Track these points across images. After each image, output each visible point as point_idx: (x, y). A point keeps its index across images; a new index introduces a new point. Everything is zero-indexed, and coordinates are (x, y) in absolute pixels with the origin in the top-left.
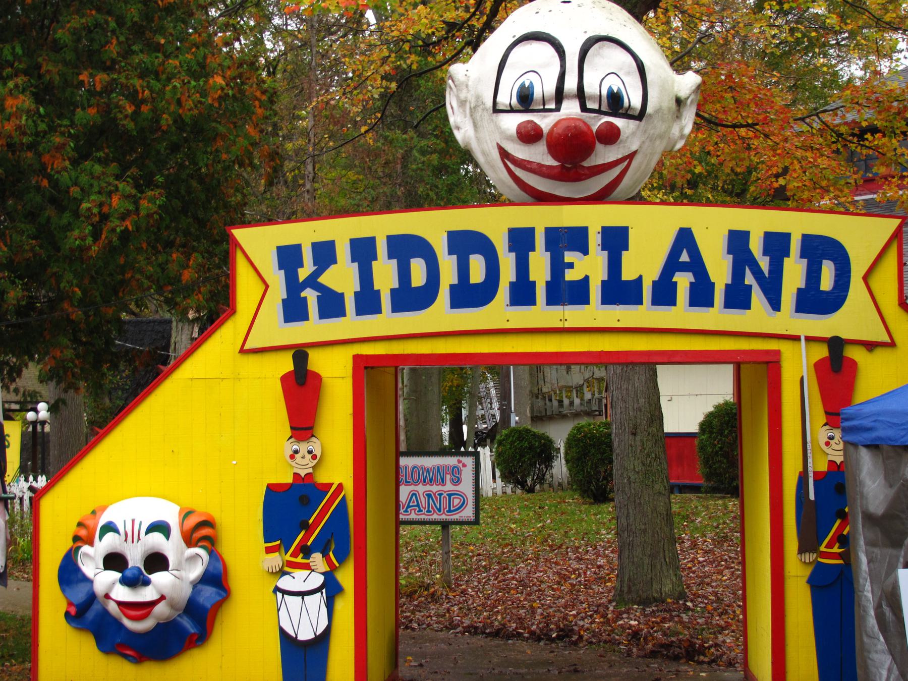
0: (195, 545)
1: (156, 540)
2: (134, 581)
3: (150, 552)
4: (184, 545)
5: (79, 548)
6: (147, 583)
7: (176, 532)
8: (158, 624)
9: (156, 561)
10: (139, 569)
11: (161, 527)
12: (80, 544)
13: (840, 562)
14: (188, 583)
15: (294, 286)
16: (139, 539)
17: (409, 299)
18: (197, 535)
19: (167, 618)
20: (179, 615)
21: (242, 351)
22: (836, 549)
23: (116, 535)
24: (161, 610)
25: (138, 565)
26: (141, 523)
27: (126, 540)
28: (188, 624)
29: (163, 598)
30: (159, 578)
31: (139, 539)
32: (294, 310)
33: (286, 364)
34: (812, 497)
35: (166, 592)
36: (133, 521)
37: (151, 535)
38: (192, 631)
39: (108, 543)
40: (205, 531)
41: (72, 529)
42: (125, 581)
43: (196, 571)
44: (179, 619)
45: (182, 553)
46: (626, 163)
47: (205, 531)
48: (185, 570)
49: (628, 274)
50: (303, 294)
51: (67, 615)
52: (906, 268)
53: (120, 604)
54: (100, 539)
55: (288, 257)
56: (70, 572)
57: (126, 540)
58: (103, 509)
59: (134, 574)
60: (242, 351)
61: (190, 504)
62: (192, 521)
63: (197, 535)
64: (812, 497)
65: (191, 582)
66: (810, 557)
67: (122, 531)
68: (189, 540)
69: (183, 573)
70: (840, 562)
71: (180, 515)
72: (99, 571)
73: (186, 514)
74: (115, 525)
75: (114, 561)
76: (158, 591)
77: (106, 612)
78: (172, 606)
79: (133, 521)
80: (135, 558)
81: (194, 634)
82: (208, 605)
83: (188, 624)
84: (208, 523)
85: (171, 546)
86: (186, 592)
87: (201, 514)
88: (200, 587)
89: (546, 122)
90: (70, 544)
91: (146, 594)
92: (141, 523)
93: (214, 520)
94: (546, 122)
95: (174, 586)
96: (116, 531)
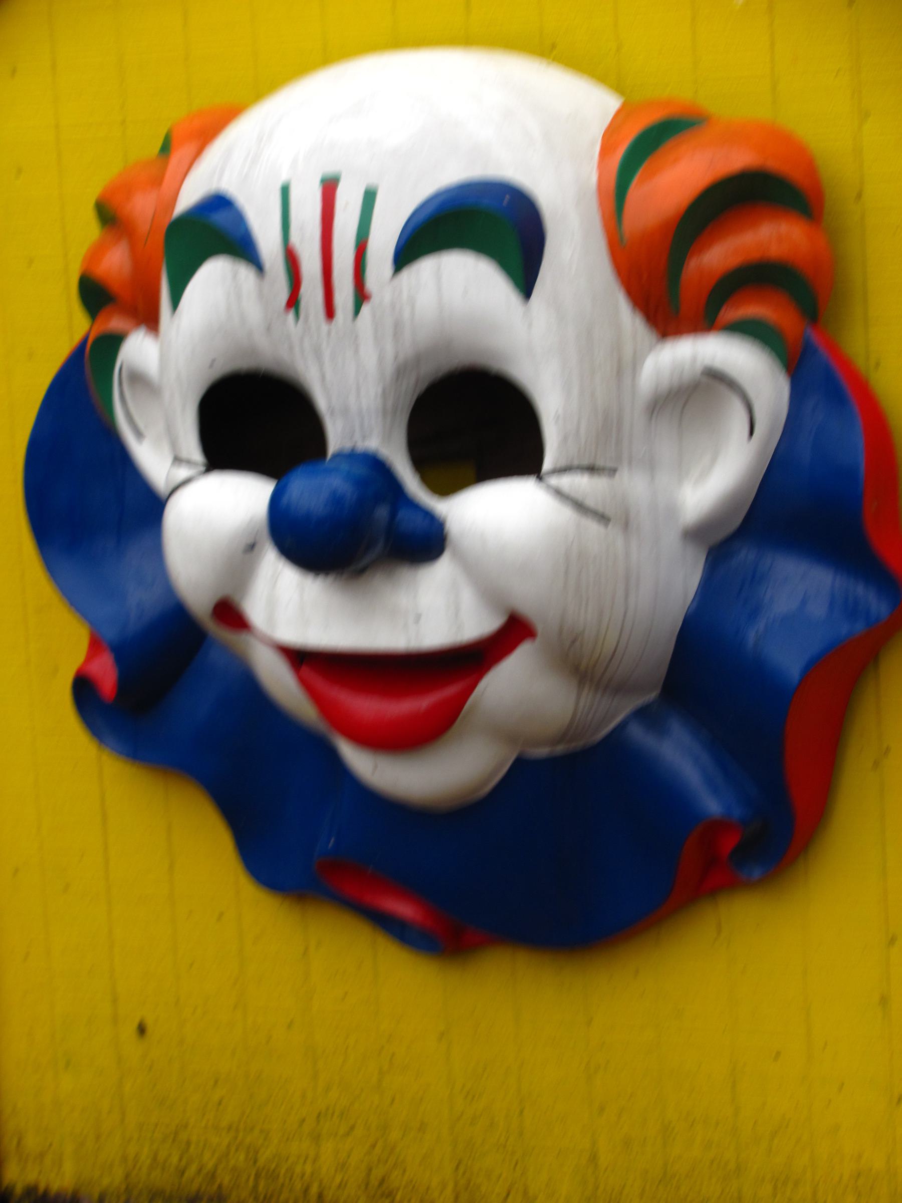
0: (705, 320)
1: (463, 286)
2: (356, 532)
3: (430, 370)
4: (629, 321)
5: (111, 343)
6: (425, 543)
7: (575, 246)
8: (522, 767)
9: (476, 420)
10: (377, 467)
11: (490, 222)
12: (116, 323)
14: (671, 540)
16: (361, 295)
18: (718, 255)
19: (563, 736)
20: (642, 714)
23: (245, 273)
24: (513, 686)
25: (373, 443)
26: (370, 197)
27: (293, 302)
28: (680, 756)
29: (514, 631)
30: (495, 514)
31: (361, 295)
35: (529, 599)
36: (329, 188)
37: (408, 274)
38: (712, 806)
39: (208, 319)
40: (770, 236)
41: (72, 239)
42: (304, 540)
43: (716, 474)
44: (638, 733)
45: (624, 369)
47: (770, 236)
48: (651, 465)
51: (83, 690)
52: (600, 463)
53: (299, 658)
54: (175, 301)
57: (293, 302)
58: (207, 128)
59: (336, 500)
61: (673, 82)
62: (680, 177)
63: (718, 255)
65: (695, 534)
67: (268, 241)
68: (664, 284)
69: (634, 485)
71: (606, 150)
72: (183, 473)
73: (645, 141)
74: (239, 219)
75: (251, 417)
76: (489, 593)
77: (249, 688)
78: (579, 665)
79: (329, 188)
80: (357, 404)
81: (717, 827)
82: (789, 660)
83: (680, 756)
84: (770, 187)
85: (555, 335)
86: (671, 583)
87: (738, 134)
88: (746, 555)
90: (72, 326)
91: (428, 611)
92: (370, 197)
93: (810, 166)
95: (571, 562)
96: (242, 247)
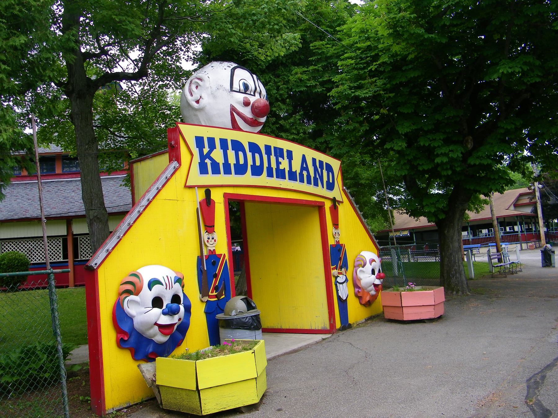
13: (216, 299)
15: (203, 157)
17: (241, 170)
21: (186, 186)
22: (215, 294)
27: (166, 288)
32: (203, 170)
33: (201, 195)
34: (205, 269)
46: (234, 113)
49: (294, 170)
50: (206, 161)
55: (199, 141)
56: (120, 315)
57: (166, 288)
60: (186, 186)
64: (205, 269)
66: (206, 299)
70: (216, 299)
89: (252, 99)
94: (252, 99)
